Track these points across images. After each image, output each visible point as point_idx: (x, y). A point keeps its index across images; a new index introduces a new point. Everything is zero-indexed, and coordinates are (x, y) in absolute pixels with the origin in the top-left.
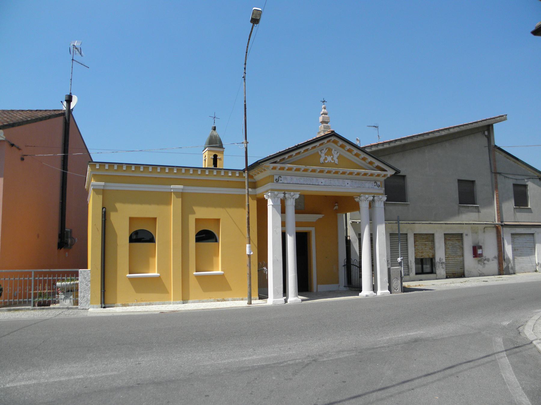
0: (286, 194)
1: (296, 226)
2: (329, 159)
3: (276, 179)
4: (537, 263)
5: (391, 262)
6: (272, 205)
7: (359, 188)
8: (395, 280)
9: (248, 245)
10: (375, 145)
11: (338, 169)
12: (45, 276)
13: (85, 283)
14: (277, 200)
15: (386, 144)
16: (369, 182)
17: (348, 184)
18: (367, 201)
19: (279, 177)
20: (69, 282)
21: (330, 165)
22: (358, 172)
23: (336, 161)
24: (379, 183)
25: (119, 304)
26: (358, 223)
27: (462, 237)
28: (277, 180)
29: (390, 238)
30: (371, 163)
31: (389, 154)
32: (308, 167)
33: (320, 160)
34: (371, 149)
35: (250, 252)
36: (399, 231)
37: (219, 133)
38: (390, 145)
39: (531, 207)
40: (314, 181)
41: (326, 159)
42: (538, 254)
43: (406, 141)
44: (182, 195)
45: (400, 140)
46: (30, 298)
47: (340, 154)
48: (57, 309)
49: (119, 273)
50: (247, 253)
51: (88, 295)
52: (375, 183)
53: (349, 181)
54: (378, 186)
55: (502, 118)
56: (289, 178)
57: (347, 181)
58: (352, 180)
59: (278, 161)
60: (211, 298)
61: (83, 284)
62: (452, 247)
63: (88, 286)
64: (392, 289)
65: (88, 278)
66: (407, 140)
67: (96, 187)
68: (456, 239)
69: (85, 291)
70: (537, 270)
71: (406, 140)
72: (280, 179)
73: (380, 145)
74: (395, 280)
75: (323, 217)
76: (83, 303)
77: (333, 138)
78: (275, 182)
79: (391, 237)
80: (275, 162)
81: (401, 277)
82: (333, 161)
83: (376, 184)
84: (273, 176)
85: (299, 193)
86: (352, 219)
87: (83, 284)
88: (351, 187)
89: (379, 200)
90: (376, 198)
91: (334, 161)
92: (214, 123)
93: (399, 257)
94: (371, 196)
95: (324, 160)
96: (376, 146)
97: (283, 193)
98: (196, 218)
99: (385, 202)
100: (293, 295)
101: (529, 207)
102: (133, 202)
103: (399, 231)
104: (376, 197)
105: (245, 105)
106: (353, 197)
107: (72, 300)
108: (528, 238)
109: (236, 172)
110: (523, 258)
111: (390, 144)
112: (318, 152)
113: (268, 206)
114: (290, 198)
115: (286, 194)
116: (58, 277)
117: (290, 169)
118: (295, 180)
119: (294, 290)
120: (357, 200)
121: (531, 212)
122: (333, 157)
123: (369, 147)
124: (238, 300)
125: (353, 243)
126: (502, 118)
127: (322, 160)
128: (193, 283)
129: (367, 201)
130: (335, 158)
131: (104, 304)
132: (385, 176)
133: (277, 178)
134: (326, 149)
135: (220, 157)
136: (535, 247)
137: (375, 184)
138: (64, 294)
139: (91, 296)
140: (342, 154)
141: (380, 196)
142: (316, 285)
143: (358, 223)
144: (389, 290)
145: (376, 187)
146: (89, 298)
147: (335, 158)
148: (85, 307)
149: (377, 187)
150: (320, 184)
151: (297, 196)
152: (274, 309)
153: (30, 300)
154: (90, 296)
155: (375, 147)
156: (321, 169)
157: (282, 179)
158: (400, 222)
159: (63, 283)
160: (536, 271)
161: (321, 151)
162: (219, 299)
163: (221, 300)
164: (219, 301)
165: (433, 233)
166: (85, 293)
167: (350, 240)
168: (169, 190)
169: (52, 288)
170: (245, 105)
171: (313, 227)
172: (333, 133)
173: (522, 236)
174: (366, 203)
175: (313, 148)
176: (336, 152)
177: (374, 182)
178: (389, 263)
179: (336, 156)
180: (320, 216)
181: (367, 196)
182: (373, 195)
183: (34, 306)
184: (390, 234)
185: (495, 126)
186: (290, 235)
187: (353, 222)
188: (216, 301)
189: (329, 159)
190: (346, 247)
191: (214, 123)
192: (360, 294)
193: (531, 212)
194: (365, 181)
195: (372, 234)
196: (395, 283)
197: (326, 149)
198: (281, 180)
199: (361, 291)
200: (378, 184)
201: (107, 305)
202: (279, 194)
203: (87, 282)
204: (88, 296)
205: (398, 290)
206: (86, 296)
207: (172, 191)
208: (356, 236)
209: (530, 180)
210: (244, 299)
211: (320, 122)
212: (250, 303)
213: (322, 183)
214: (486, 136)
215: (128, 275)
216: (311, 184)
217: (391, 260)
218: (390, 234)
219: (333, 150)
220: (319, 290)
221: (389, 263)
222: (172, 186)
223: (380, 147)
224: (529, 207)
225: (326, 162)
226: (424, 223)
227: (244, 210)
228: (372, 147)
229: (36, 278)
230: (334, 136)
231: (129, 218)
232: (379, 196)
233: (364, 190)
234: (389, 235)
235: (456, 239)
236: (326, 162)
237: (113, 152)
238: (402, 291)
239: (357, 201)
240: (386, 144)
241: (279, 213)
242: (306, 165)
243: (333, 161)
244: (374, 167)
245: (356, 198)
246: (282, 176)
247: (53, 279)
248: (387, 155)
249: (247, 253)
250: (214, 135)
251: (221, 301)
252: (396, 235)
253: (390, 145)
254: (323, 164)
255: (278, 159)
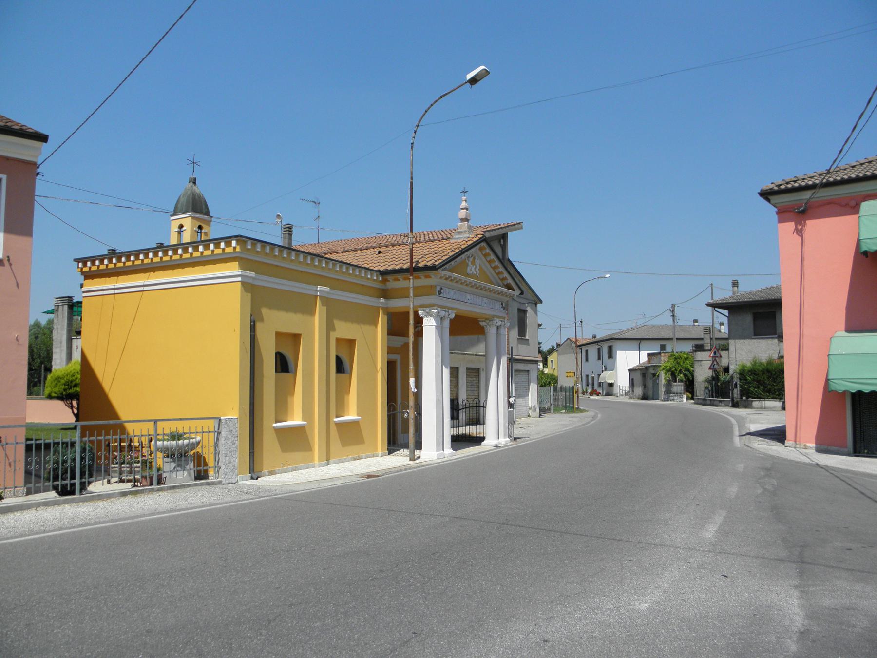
1: (388, 353)
4: (530, 406)
6: (436, 326)
12: (99, 434)
13: (231, 441)
20: (175, 442)
25: (265, 471)
27: (478, 373)
30: (505, 279)
37: (201, 189)
39: (529, 337)
42: (532, 396)
44: (326, 301)
46: (74, 478)
48: (193, 486)
49: (265, 422)
51: (234, 459)
55: (517, 226)
60: (348, 456)
61: (228, 442)
62: (471, 385)
63: (234, 444)
65: (234, 430)
67: (246, 280)
68: (475, 375)
69: (231, 454)
70: (530, 414)
76: (228, 473)
87: (228, 442)
92: (194, 171)
98: (337, 337)
101: (527, 338)
102: (287, 309)
105: (412, 183)
106: (477, 319)
107: (192, 472)
108: (524, 375)
109: (775, 312)
110: (520, 400)
113: (424, 327)
116: (89, 437)
120: (482, 324)
121: (528, 344)
126: (517, 226)
128: (269, 442)
131: (254, 472)
135: (206, 231)
136: (529, 388)
138: (174, 461)
139: (239, 461)
146: (236, 463)
148: (230, 481)
151: (453, 316)
152: (499, 454)
153: (72, 481)
154: (237, 460)
159: (180, 442)
160: (529, 416)
166: (231, 457)
168: (313, 293)
169: (42, 461)
170: (412, 183)
171: (398, 354)
173: (521, 374)
183: (151, 484)
185: (510, 234)
191: (194, 171)
192: (482, 443)
193: (528, 344)
195: (457, 368)
201: (259, 474)
203: (233, 439)
204: (235, 461)
206: (232, 461)
207: (318, 294)
209: (530, 304)
211: (460, 219)
214: (501, 245)
215: (275, 425)
222: (319, 288)
224: (527, 338)
227: (374, 327)
229: (84, 439)
231: (274, 334)
235: (475, 375)
237: (155, 211)
245: (481, 321)
247: (105, 440)
250: (197, 193)
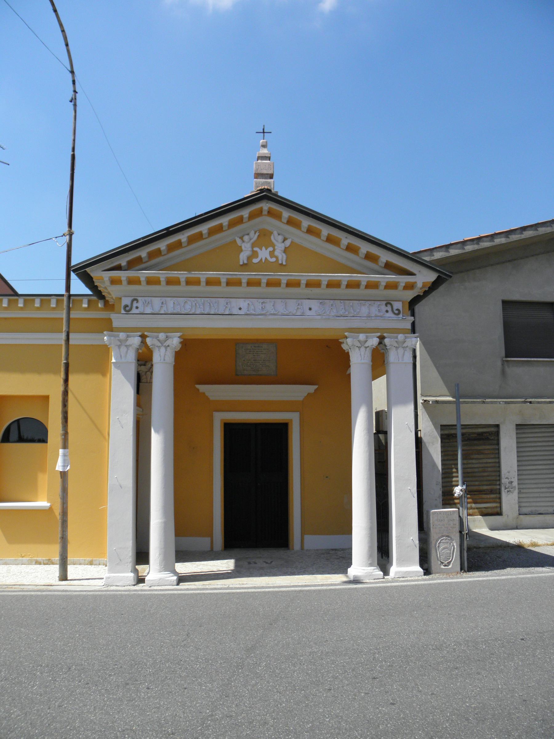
0: (147, 336)
2: (264, 254)
3: (126, 306)
5: (518, 484)
7: (342, 318)
8: (444, 541)
9: (61, 451)
10: (472, 240)
11: (275, 275)
14: (127, 352)
15: (499, 236)
16: (370, 302)
17: (310, 309)
18: (363, 349)
19: (133, 301)
21: (264, 266)
22: (331, 279)
23: (282, 257)
24: (398, 305)
26: (431, 402)
28: (127, 309)
29: (517, 433)
31: (515, 260)
32: (195, 274)
33: (239, 259)
34: (464, 249)
35: (64, 466)
36: (458, 417)
38: (509, 238)
40: (221, 305)
41: (255, 254)
43: (549, 228)
45: (533, 228)
47: (292, 242)
50: (57, 469)
52: (386, 306)
53: (315, 304)
54: (396, 312)
56: (157, 302)
57: (307, 303)
58: (321, 301)
59: (124, 263)
60: (23, 557)
64: (434, 563)
66: (551, 226)
71: (547, 227)
72: (135, 304)
73: (485, 239)
74: (444, 541)
75: (316, 390)
77: (265, 206)
78: (123, 312)
79: (519, 431)
80: (118, 268)
81: (461, 532)
82: (273, 260)
83: (389, 308)
84: (121, 299)
85: (179, 334)
86: (426, 396)
88: (319, 317)
89: (396, 345)
90: (387, 341)
91: (277, 258)
93: (457, 486)
94: (372, 337)
95: (249, 258)
96: (475, 242)
97: (140, 336)
99: (505, 359)
100: (158, 568)
103: (458, 417)
104: (389, 337)
109: (82, 300)
111: (510, 236)
112: (235, 241)
114: (157, 346)
115: (147, 336)
117: (150, 281)
118: (171, 305)
119: (160, 554)
122: (274, 250)
123: (459, 245)
124: (80, 564)
125: (427, 445)
127: (243, 257)
129: (363, 349)
130: (277, 250)
132: (410, 286)
133: (129, 304)
134: (255, 233)
137: (386, 308)
140: (297, 241)
141: (401, 337)
142: (300, 536)
143: (431, 402)
144: (421, 565)
145: (390, 314)
147: (279, 253)
149: (393, 315)
150: (235, 311)
155: (474, 244)
156: (229, 277)
157: (140, 304)
158: (461, 400)
161: (241, 238)
162: (39, 559)
163: (45, 562)
164: (40, 564)
165: (497, 423)
167: (421, 438)
172: (263, 192)
174: (362, 353)
175: (212, 232)
176: (280, 238)
177: (384, 302)
178: (515, 487)
179: (280, 247)
180: (311, 389)
181: (362, 337)
182: (379, 334)
184: (517, 425)
186: (156, 431)
187: (425, 401)
188: (34, 562)
189: (264, 254)
190: (416, 452)
194: (357, 302)
196: (444, 549)
197: (255, 233)
198: (137, 308)
199: (349, 564)
200: (395, 308)
202: (129, 339)
205: (450, 567)
208: (434, 430)
210: (94, 562)
212: (64, 577)
213: (240, 309)
216: (212, 313)
217: (518, 479)
218: (517, 425)
219: (275, 233)
220: (306, 547)
221: (515, 487)
223: (486, 244)
225: (255, 261)
226: (545, 402)
228: (466, 246)
230: (266, 201)
232: (396, 335)
233: (356, 324)
234: (515, 427)
236: (255, 261)
238: (462, 569)
239: (346, 352)
240: (501, 238)
241: (128, 380)
242: (189, 271)
243: (273, 260)
244: (381, 267)
246: (139, 299)
248: (509, 261)
249: (57, 469)
251: (44, 564)
252: (542, 428)
253: (509, 238)
254: (245, 267)
255: (123, 261)
